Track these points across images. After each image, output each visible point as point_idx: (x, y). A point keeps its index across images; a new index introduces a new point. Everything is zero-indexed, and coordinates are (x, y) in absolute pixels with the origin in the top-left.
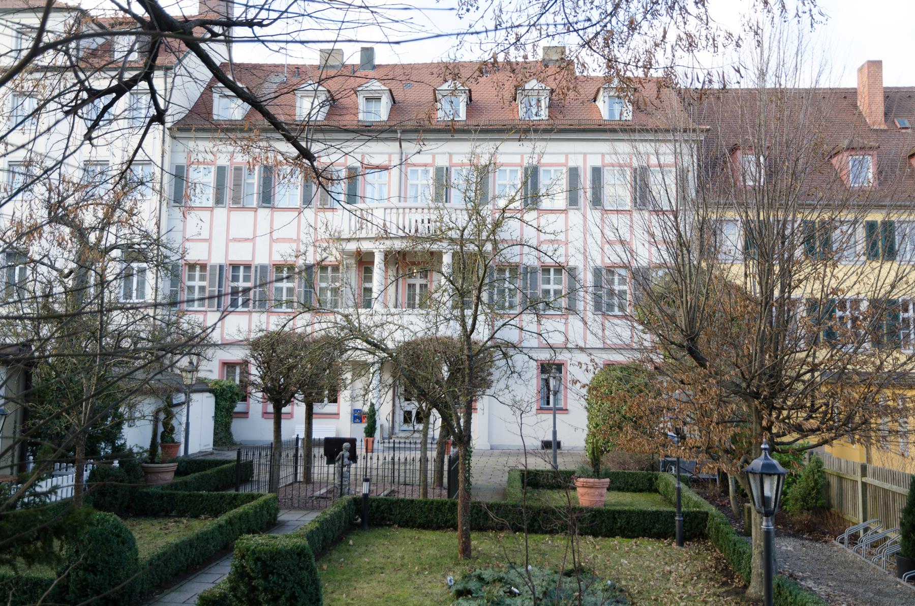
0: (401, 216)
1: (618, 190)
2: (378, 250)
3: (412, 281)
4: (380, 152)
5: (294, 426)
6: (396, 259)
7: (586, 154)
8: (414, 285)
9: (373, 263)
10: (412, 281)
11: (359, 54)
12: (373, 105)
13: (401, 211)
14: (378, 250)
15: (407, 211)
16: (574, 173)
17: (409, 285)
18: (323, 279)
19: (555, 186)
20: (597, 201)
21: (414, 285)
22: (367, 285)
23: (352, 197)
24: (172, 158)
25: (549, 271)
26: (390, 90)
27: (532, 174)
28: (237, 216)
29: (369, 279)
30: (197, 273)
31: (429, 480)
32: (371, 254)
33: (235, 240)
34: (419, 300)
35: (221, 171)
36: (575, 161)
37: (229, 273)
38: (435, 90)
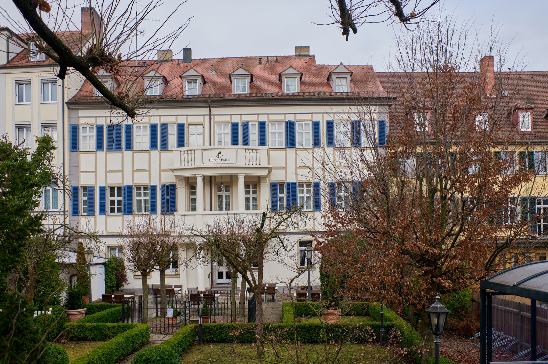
0: (190, 155)
1: (342, 135)
2: (199, 175)
3: (220, 194)
4: (196, 115)
5: (154, 279)
6: (210, 181)
7: (322, 114)
8: (222, 196)
9: (196, 183)
10: (220, 194)
11: (182, 53)
12: (192, 85)
13: (186, 152)
14: (199, 175)
15: (189, 152)
16: (316, 125)
17: (219, 196)
18: (302, 192)
19: (304, 135)
20: (330, 142)
21: (222, 196)
22: (193, 197)
23: (181, 143)
24: (69, 121)
25: (140, 188)
26: (202, 76)
27: (291, 127)
28: (164, 155)
29: (194, 193)
30: (142, 191)
31: (246, 307)
32: (195, 178)
33: (111, 171)
34: (225, 204)
35: (100, 129)
36: (316, 118)
37: (108, 192)
38: (230, 75)
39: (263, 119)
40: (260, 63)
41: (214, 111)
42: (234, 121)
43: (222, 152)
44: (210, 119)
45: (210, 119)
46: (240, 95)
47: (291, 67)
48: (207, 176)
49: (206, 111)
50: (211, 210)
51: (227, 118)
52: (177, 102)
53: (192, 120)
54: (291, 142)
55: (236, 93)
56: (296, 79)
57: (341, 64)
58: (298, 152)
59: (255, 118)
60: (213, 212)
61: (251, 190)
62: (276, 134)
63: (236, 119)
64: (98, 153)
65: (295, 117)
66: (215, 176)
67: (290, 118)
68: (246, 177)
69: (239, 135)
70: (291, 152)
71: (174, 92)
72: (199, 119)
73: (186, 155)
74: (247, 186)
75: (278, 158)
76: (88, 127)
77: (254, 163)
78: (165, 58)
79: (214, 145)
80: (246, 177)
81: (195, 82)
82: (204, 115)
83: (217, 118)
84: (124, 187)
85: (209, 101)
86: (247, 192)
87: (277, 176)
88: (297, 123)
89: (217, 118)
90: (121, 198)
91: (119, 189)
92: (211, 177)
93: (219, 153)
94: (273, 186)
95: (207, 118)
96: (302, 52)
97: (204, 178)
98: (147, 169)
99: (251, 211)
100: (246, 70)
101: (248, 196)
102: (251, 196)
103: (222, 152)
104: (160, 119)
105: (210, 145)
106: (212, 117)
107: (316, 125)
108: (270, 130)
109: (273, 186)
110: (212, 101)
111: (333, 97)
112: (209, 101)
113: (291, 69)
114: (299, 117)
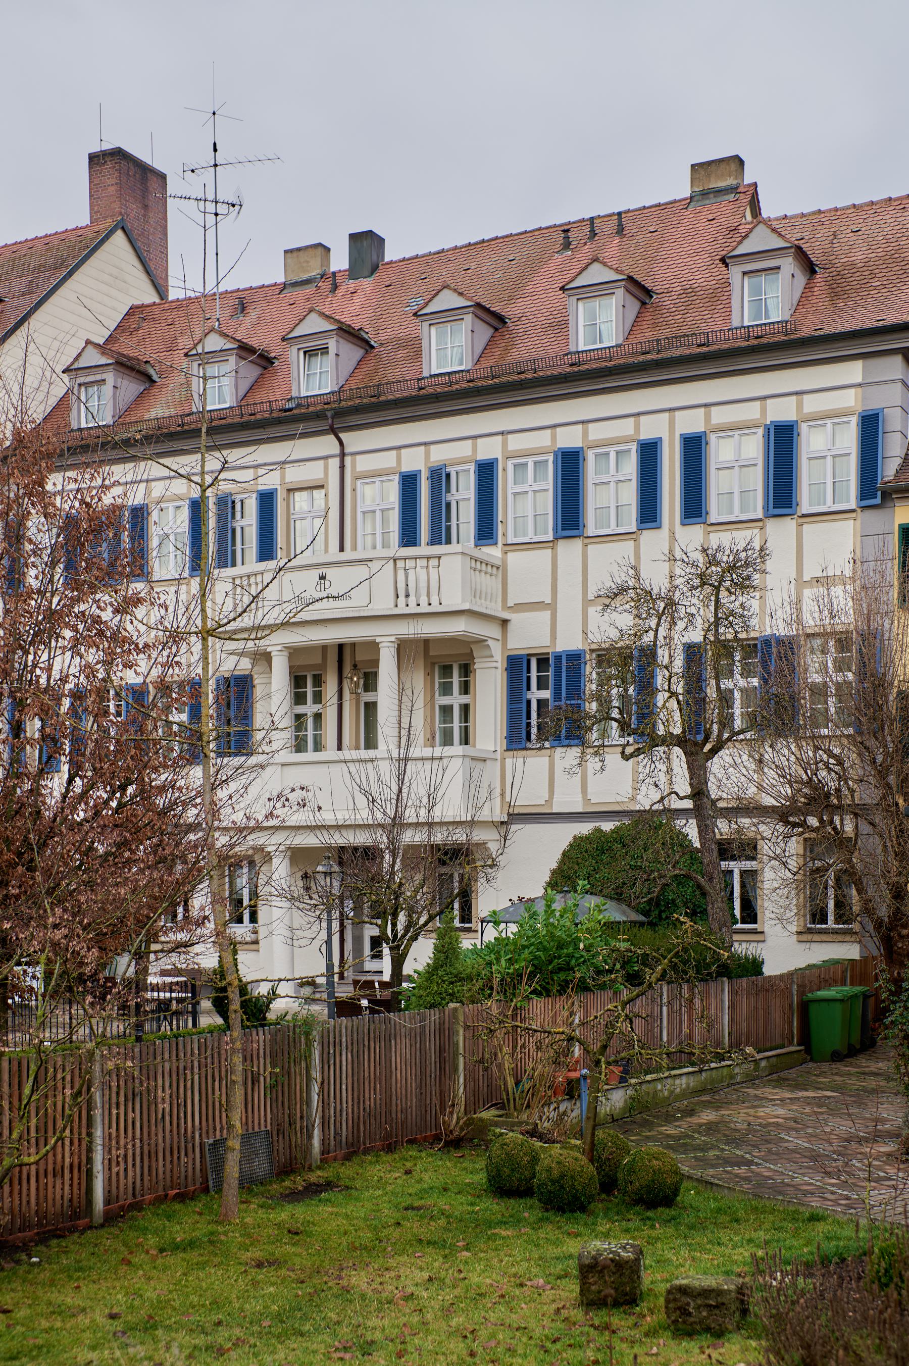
4: (302, 460)
9: (376, 662)
14: (385, 637)
16: (649, 453)
19: (610, 492)
27: (782, 441)
32: (373, 646)
36: (650, 429)
39: (488, 450)
40: (567, 245)
41: (354, 440)
42: (407, 467)
43: (330, 573)
44: (342, 467)
45: (342, 467)
46: (454, 378)
47: (595, 260)
48: (333, 646)
49: (327, 444)
50: (340, 748)
51: (751, 412)
52: (437, 398)
53: (294, 475)
54: (570, 517)
55: (581, 348)
56: (614, 299)
57: (88, 342)
58: (809, 529)
59: (464, 449)
60: (347, 754)
61: (310, 690)
62: (528, 502)
63: (415, 461)
64: (562, 545)
65: (800, 406)
66: (353, 645)
67: (570, 439)
68: (294, 652)
69: (421, 512)
70: (570, 550)
71: (529, 349)
72: (312, 472)
73: (422, 573)
74: (298, 681)
75: (528, 572)
76: (530, 461)
77: (435, 600)
78: (308, 273)
79: (354, 548)
80: (294, 652)
81: (325, 350)
82: (326, 458)
83: (364, 464)
84: (558, 658)
85: (329, 414)
86: (299, 699)
87: (530, 635)
88: (590, 455)
89: (364, 464)
90: (546, 694)
91: (543, 662)
92: (341, 647)
93: (323, 577)
94: (517, 667)
95: (335, 463)
96: (721, 181)
97: (403, 647)
98: (548, 601)
99: (310, 755)
100: (461, 294)
101: (300, 709)
102: (456, 700)
103: (330, 573)
104: (427, 455)
105: (342, 549)
106: (348, 459)
107: (649, 453)
108: (506, 484)
109: (517, 667)
110: (340, 413)
111: (765, 341)
112: (329, 414)
113: (596, 266)
114: (597, 432)
